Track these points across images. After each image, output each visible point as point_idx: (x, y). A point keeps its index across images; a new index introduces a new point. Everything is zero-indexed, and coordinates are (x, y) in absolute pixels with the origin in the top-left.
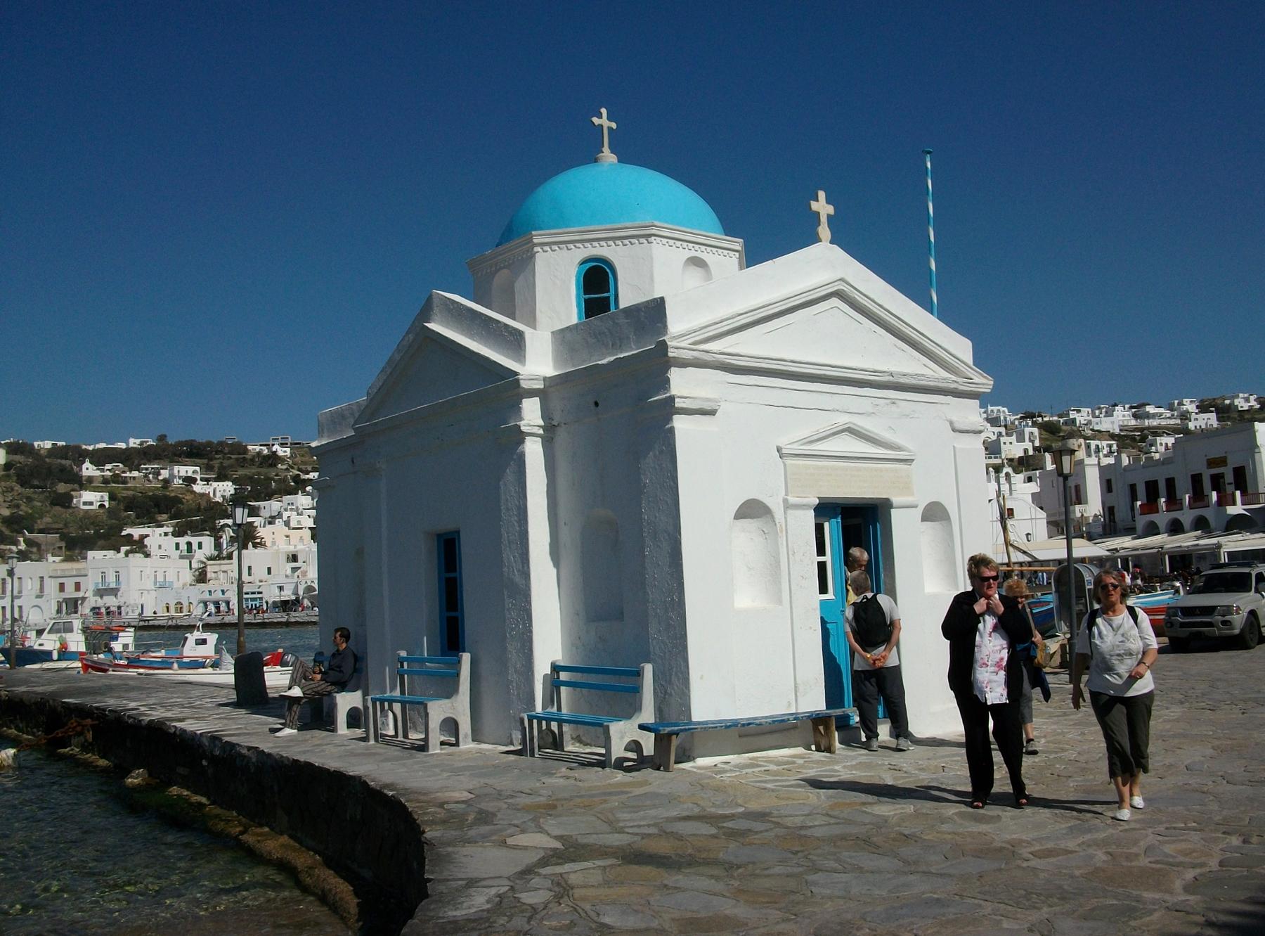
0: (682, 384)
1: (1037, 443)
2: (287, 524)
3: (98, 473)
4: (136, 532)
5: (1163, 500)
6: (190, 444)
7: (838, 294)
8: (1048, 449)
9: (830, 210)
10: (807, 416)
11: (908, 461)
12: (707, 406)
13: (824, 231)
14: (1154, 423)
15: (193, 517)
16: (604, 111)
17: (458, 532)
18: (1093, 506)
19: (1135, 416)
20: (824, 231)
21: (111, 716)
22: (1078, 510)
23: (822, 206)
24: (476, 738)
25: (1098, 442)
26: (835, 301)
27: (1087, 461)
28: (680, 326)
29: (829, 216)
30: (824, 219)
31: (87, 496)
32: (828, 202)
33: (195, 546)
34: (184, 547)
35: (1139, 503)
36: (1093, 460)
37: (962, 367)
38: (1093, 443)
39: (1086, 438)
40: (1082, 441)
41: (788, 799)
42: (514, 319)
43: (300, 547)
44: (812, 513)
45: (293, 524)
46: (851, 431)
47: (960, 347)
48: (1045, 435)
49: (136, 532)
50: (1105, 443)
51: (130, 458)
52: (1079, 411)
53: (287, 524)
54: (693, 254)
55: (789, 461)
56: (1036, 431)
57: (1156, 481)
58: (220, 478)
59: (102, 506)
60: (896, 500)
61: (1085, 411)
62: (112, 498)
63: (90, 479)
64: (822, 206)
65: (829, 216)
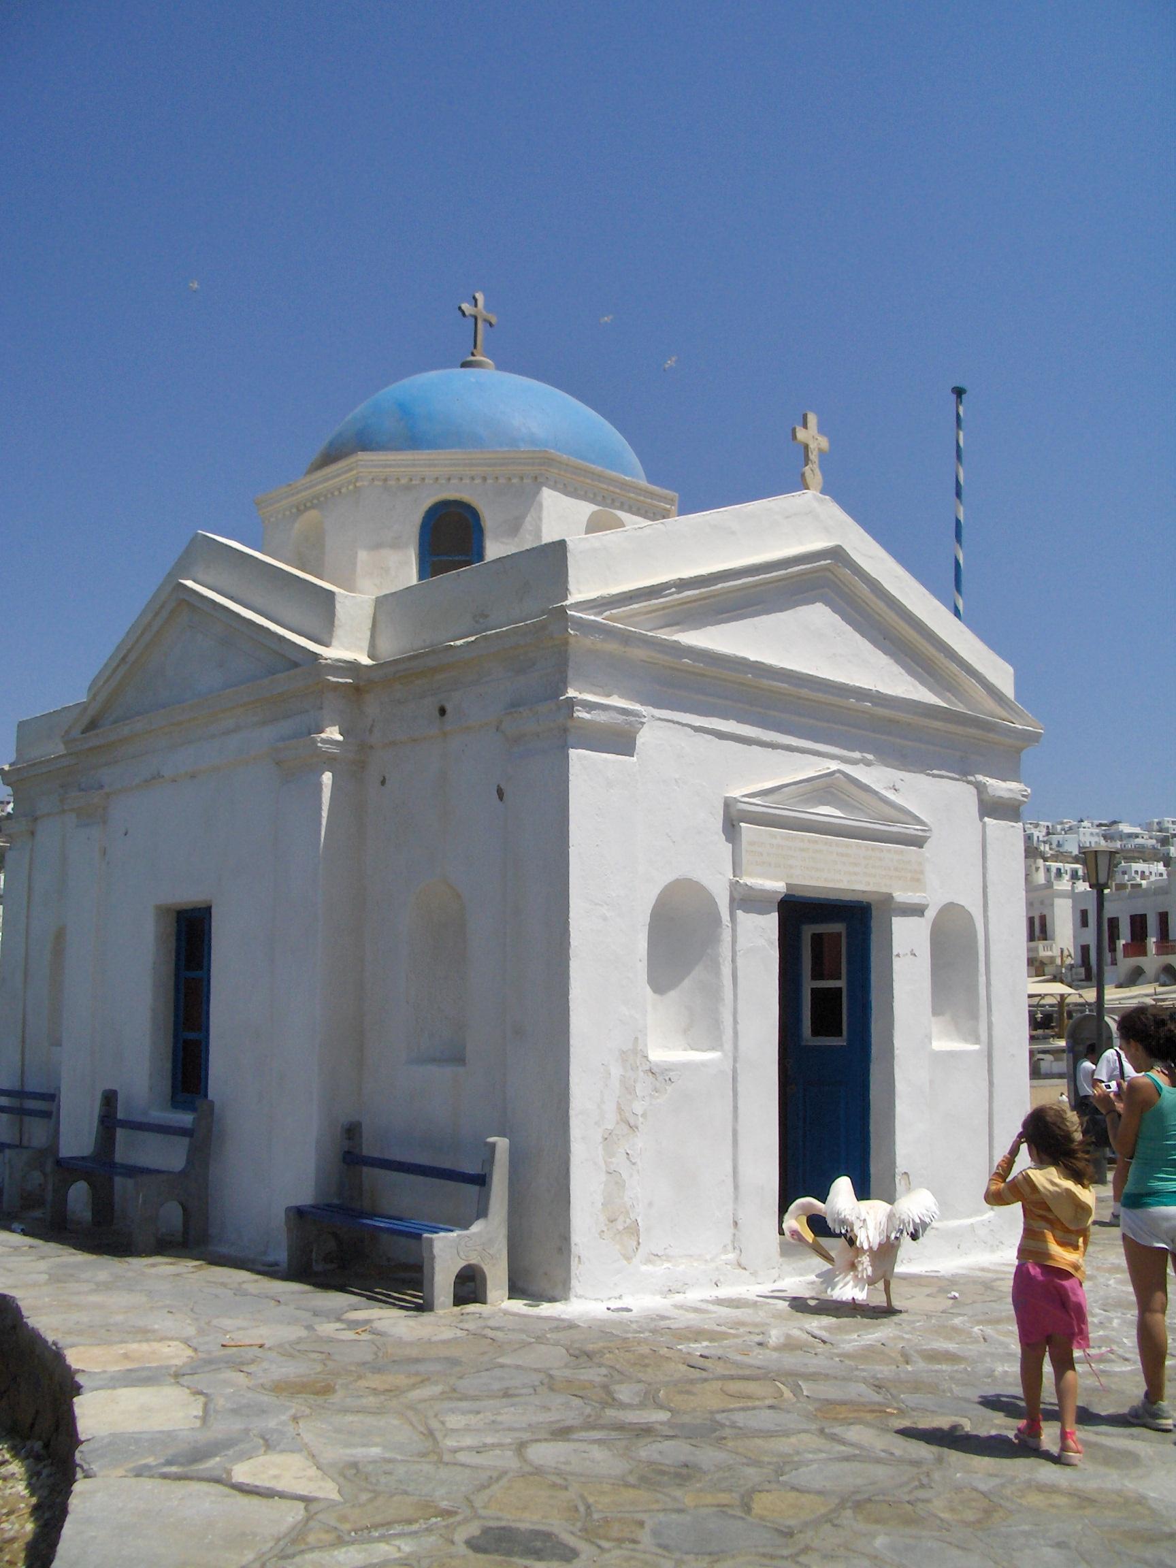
5: (1154, 939)
9: (824, 443)
13: (814, 474)
14: (1131, 844)
17: (208, 910)
19: (1105, 837)
20: (814, 474)
21: (15, 1225)
23: (812, 436)
24: (515, 1291)
25: (1060, 865)
29: (821, 452)
30: (814, 456)
32: (821, 430)
35: (1123, 942)
38: (1054, 865)
39: (1045, 860)
40: (1040, 862)
41: (162, 607)
50: (1069, 867)
52: (1037, 826)
57: (484, 1302)
64: (812, 436)
65: (821, 452)
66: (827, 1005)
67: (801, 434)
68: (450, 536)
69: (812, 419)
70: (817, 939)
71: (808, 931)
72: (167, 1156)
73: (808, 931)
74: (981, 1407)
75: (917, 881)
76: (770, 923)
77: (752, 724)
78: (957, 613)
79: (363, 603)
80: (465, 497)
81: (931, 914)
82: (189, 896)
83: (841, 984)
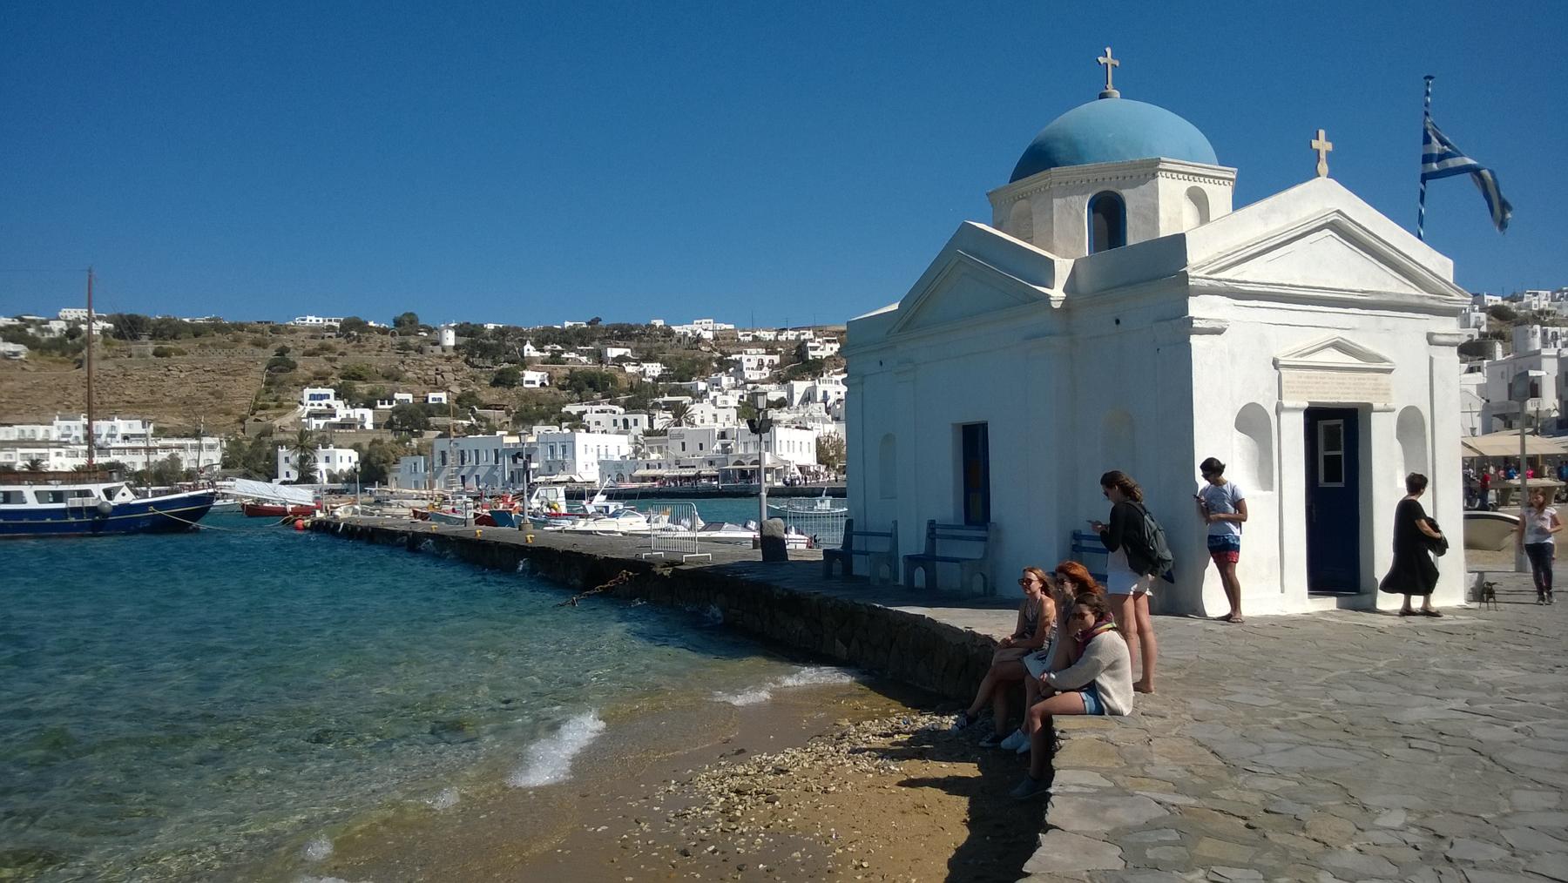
0: (1197, 308)
1: (1484, 329)
2: (714, 402)
3: (538, 354)
4: (574, 409)
6: (620, 327)
7: (1333, 226)
8: (1499, 336)
9: (1329, 146)
10: (1301, 332)
11: (1390, 371)
12: (1217, 325)
13: (1323, 167)
15: (639, 398)
16: (1108, 50)
18: (1549, 402)
20: (1323, 167)
22: (1531, 406)
23: (1322, 144)
26: (1327, 232)
27: (1545, 352)
28: (1197, 255)
30: (1323, 156)
31: (529, 375)
32: (1327, 139)
33: (631, 423)
34: (620, 423)
36: (1552, 351)
37: (1444, 287)
38: (1550, 330)
39: (1542, 324)
40: (1538, 327)
42: (1029, 240)
43: (728, 425)
44: (1302, 415)
45: (719, 403)
46: (1338, 346)
47: (1440, 265)
48: (1495, 321)
49: (574, 409)
51: (570, 339)
53: (714, 402)
54: (1193, 184)
55: (1283, 371)
56: (1483, 316)
58: (650, 359)
59: (543, 385)
60: (1376, 406)
61: (1543, 294)
62: (550, 379)
63: (532, 360)
64: (1322, 144)
66: (1332, 463)
67: (1315, 144)
68: (1109, 216)
69: (1322, 133)
70: (1327, 428)
71: (1321, 424)
72: (974, 551)
73: (1321, 424)
74: (1239, 212)
75: (1387, 393)
76: (1300, 418)
77: (948, 628)
78: (1419, 237)
79: (1065, 256)
80: (1112, 188)
81: (1397, 413)
82: (971, 418)
83: (1341, 453)
